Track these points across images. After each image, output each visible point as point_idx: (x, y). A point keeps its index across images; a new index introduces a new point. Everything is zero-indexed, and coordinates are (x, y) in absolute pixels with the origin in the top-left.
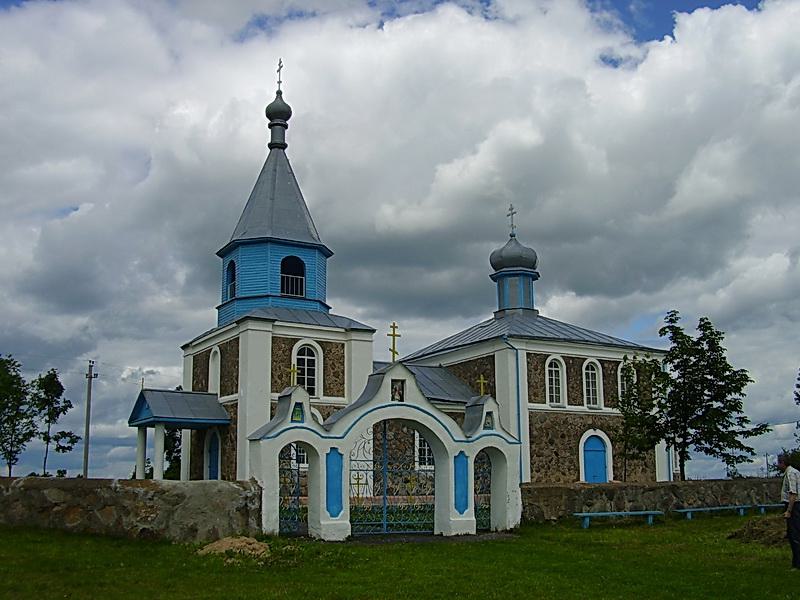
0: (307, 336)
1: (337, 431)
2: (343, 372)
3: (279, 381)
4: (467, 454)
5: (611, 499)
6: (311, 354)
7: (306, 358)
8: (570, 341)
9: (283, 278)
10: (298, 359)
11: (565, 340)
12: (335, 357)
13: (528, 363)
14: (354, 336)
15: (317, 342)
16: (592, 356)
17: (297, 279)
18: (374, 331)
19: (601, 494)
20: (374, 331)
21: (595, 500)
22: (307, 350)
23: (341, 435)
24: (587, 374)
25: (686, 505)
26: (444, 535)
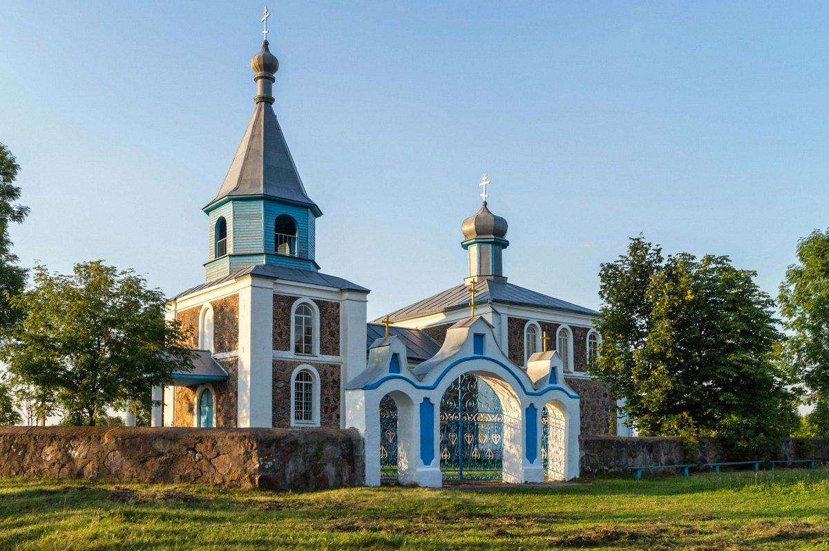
0: (306, 294)
1: (430, 381)
2: (338, 332)
3: (279, 338)
4: (536, 406)
5: (650, 452)
6: (307, 313)
7: (304, 316)
8: (201, 287)
9: (276, 236)
10: (296, 317)
11: (567, 309)
12: (330, 313)
13: (509, 327)
14: (346, 295)
15: (315, 301)
16: (565, 321)
17: (281, 236)
18: (368, 292)
19: (643, 447)
20: (368, 292)
21: (638, 453)
22: (304, 309)
23: (431, 384)
24: (590, 343)
25: (708, 459)
26: (529, 482)
